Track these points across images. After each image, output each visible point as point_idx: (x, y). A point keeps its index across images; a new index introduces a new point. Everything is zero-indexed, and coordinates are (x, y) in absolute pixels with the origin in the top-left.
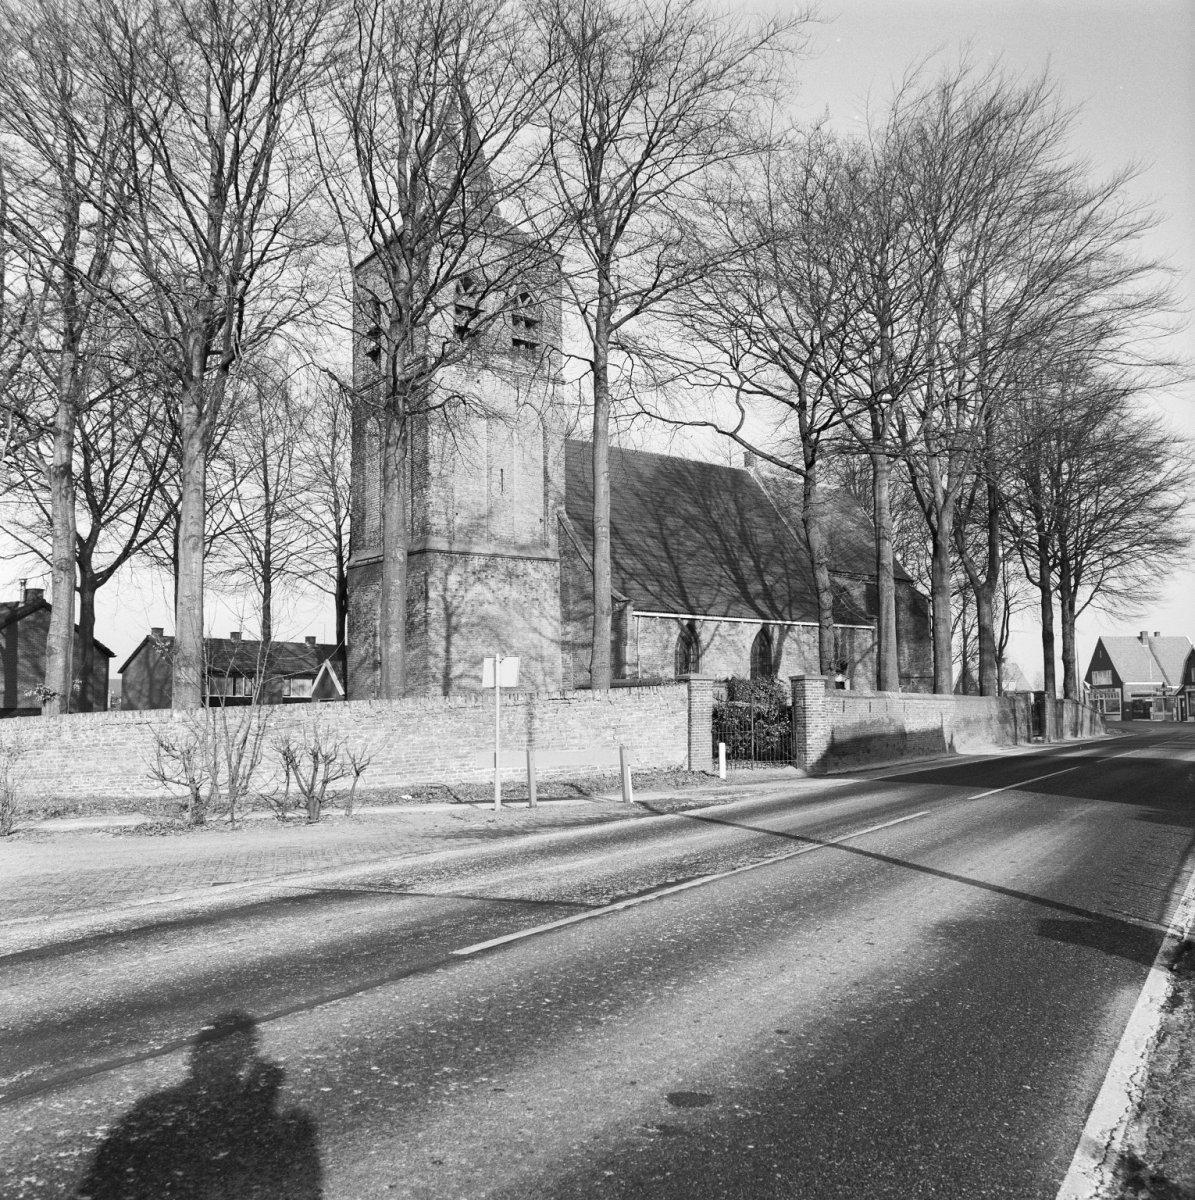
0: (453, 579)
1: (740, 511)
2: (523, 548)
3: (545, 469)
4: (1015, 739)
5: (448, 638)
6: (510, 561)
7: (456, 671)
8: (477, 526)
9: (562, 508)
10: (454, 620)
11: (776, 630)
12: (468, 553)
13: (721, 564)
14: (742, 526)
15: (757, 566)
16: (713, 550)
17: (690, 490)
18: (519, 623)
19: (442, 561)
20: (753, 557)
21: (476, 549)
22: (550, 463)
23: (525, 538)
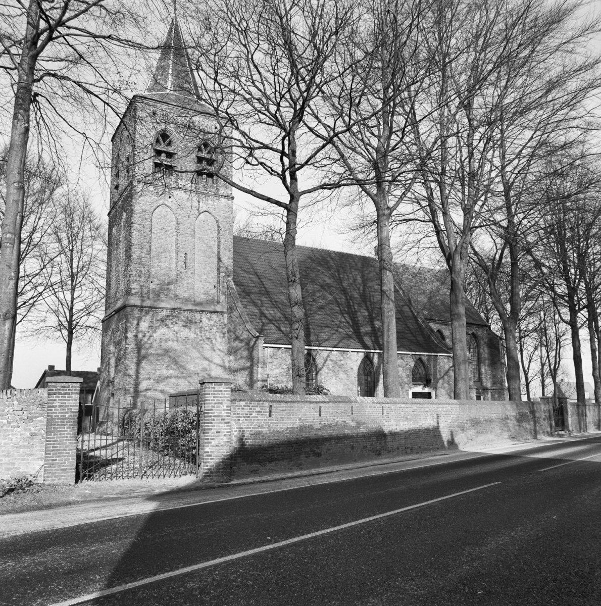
0: (144, 325)
1: (365, 281)
2: (200, 304)
3: (219, 253)
4: (535, 434)
5: (138, 364)
6: (190, 312)
7: (143, 385)
8: (165, 288)
9: (230, 279)
10: (143, 352)
11: (376, 356)
12: (155, 308)
13: (342, 314)
14: (364, 291)
15: (370, 315)
16: (339, 305)
17: (329, 269)
18: (195, 354)
19: (136, 313)
20: (368, 310)
21: (163, 305)
22: (222, 250)
23: (201, 297)
